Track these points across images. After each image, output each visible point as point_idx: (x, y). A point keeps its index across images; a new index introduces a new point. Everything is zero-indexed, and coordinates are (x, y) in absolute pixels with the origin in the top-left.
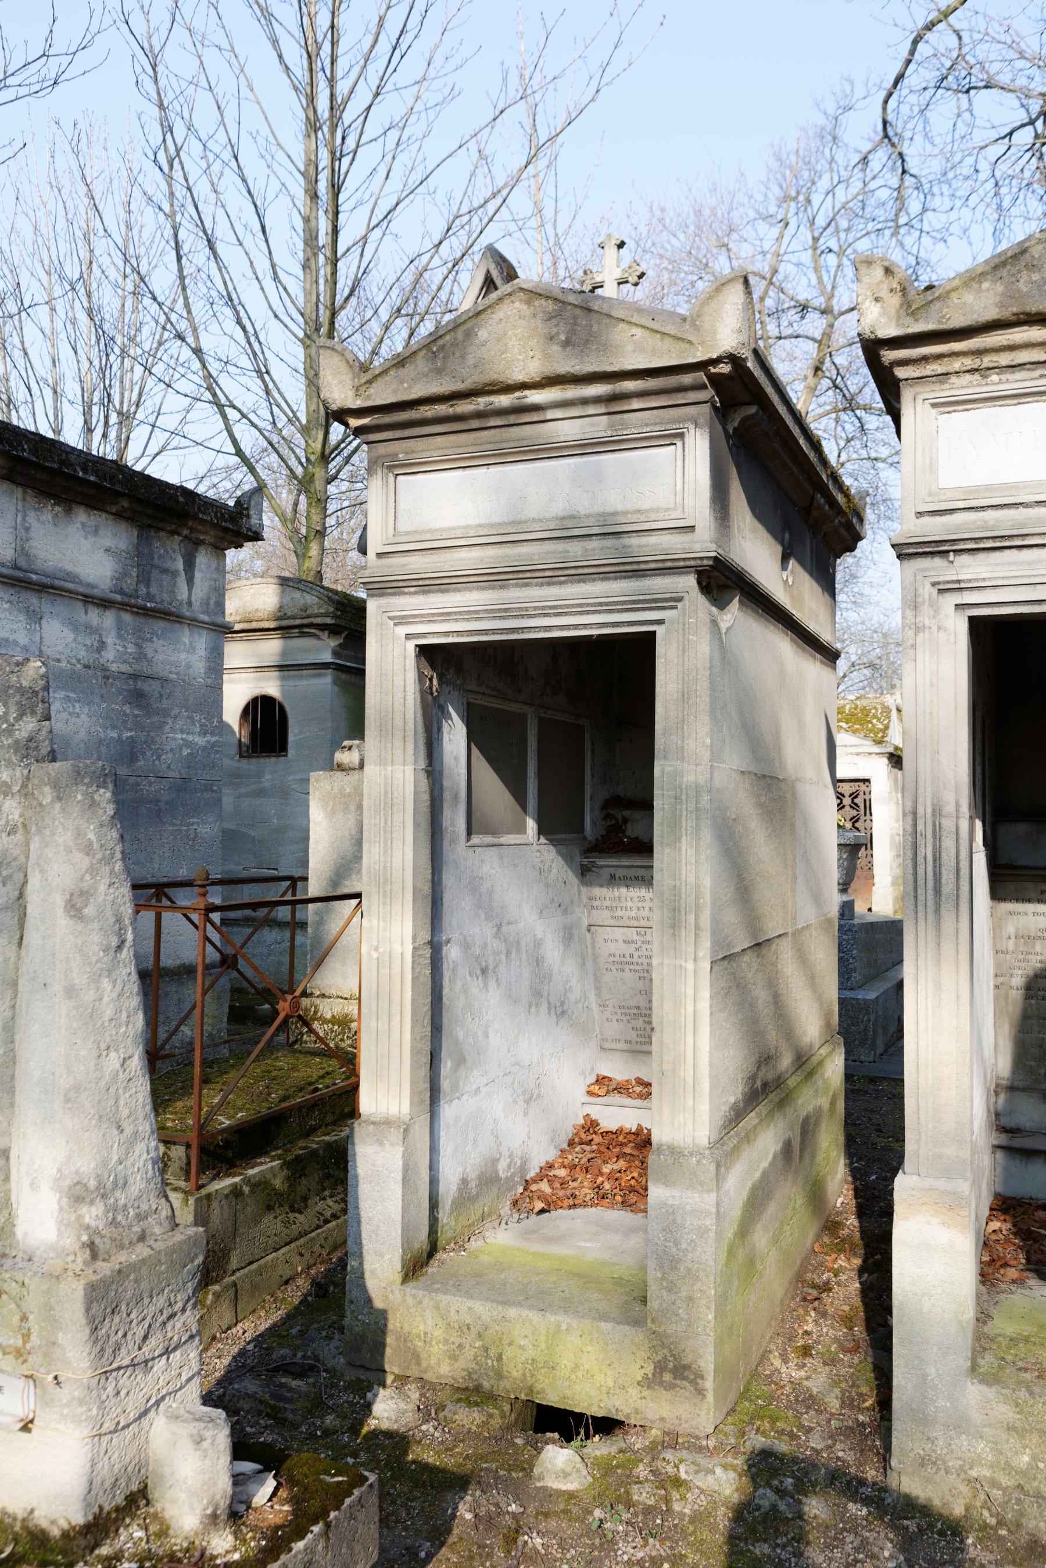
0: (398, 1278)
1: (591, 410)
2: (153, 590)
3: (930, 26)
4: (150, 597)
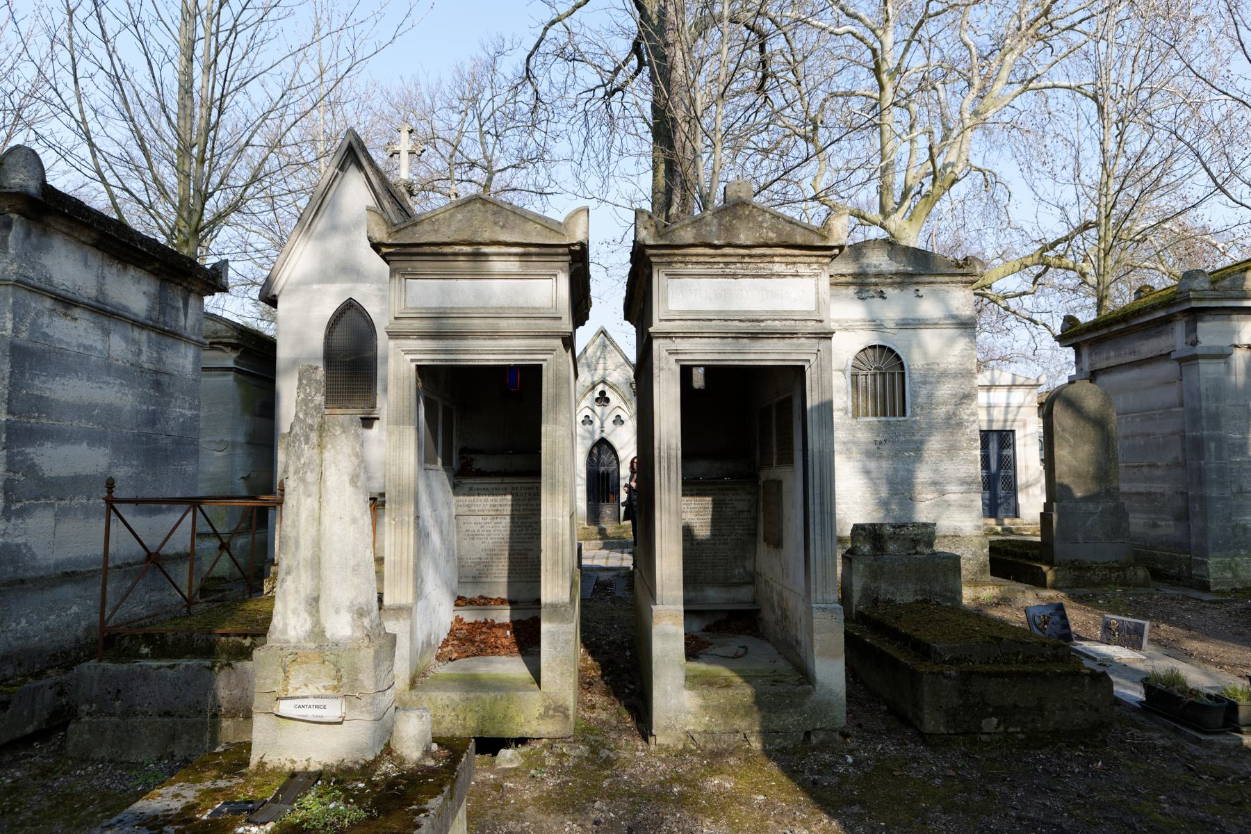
0: (408, 688)
1: (512, 258)
2: (167, 319)
3: (553, 23)
4: (165, 323)
